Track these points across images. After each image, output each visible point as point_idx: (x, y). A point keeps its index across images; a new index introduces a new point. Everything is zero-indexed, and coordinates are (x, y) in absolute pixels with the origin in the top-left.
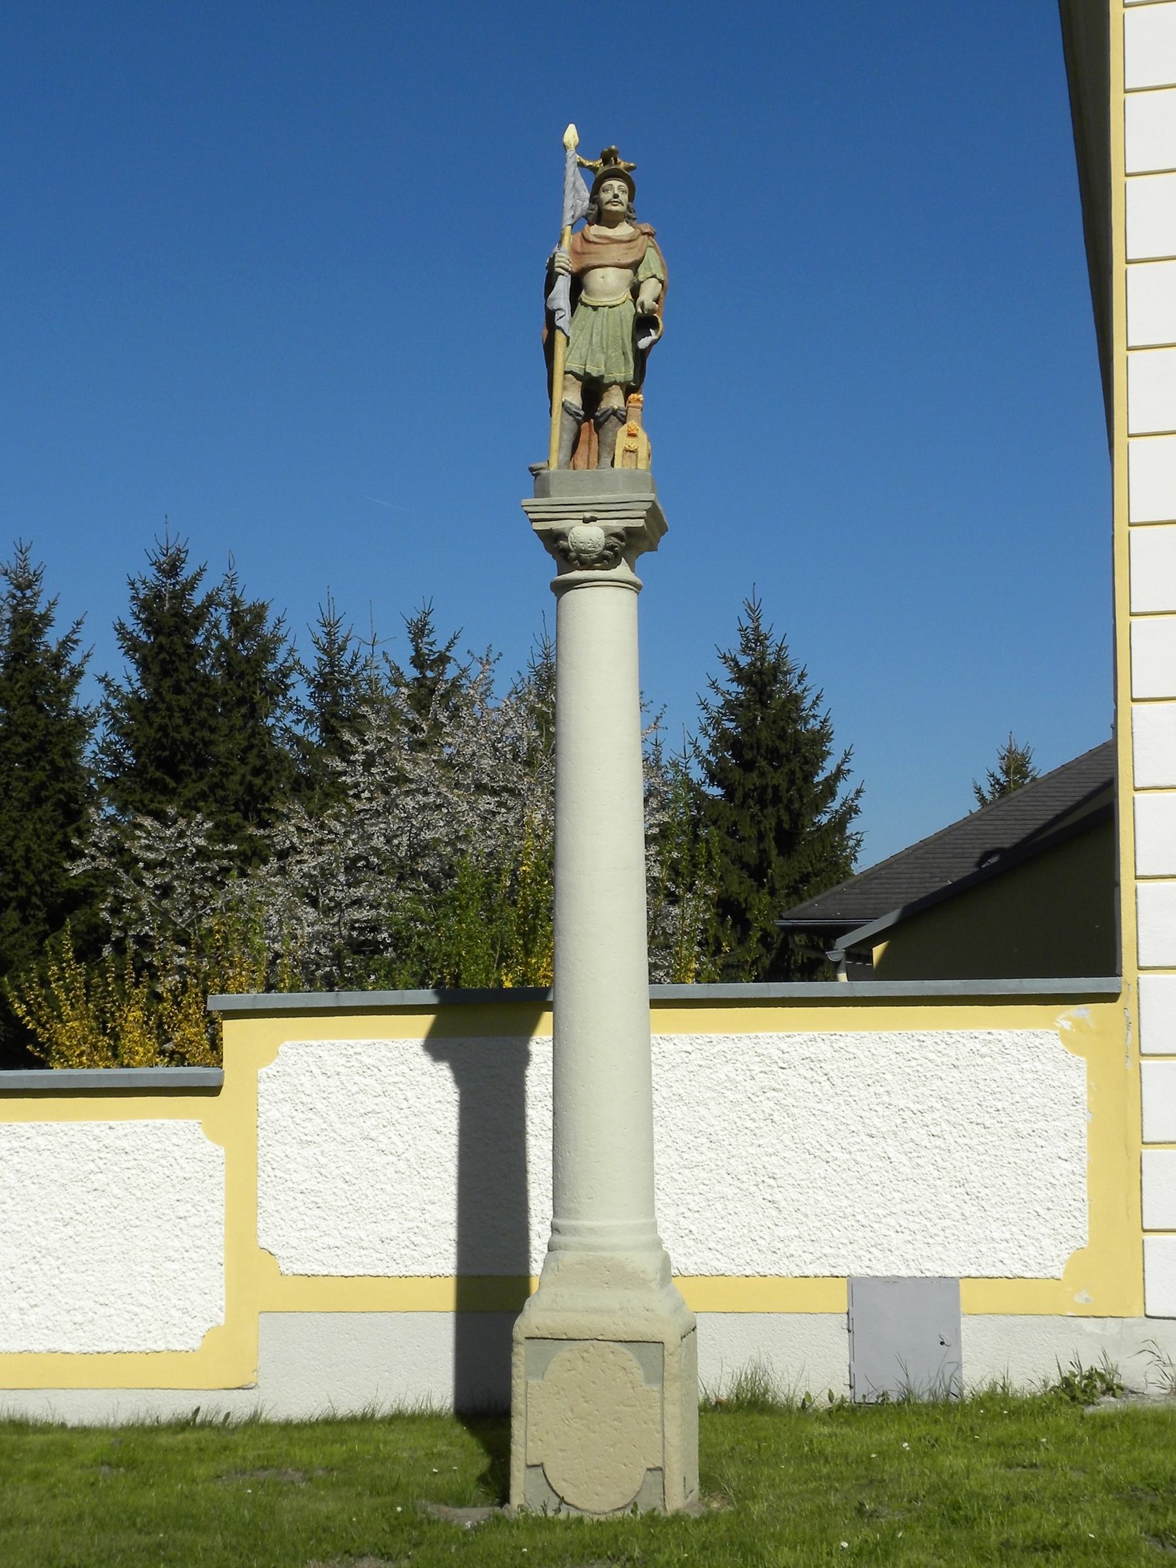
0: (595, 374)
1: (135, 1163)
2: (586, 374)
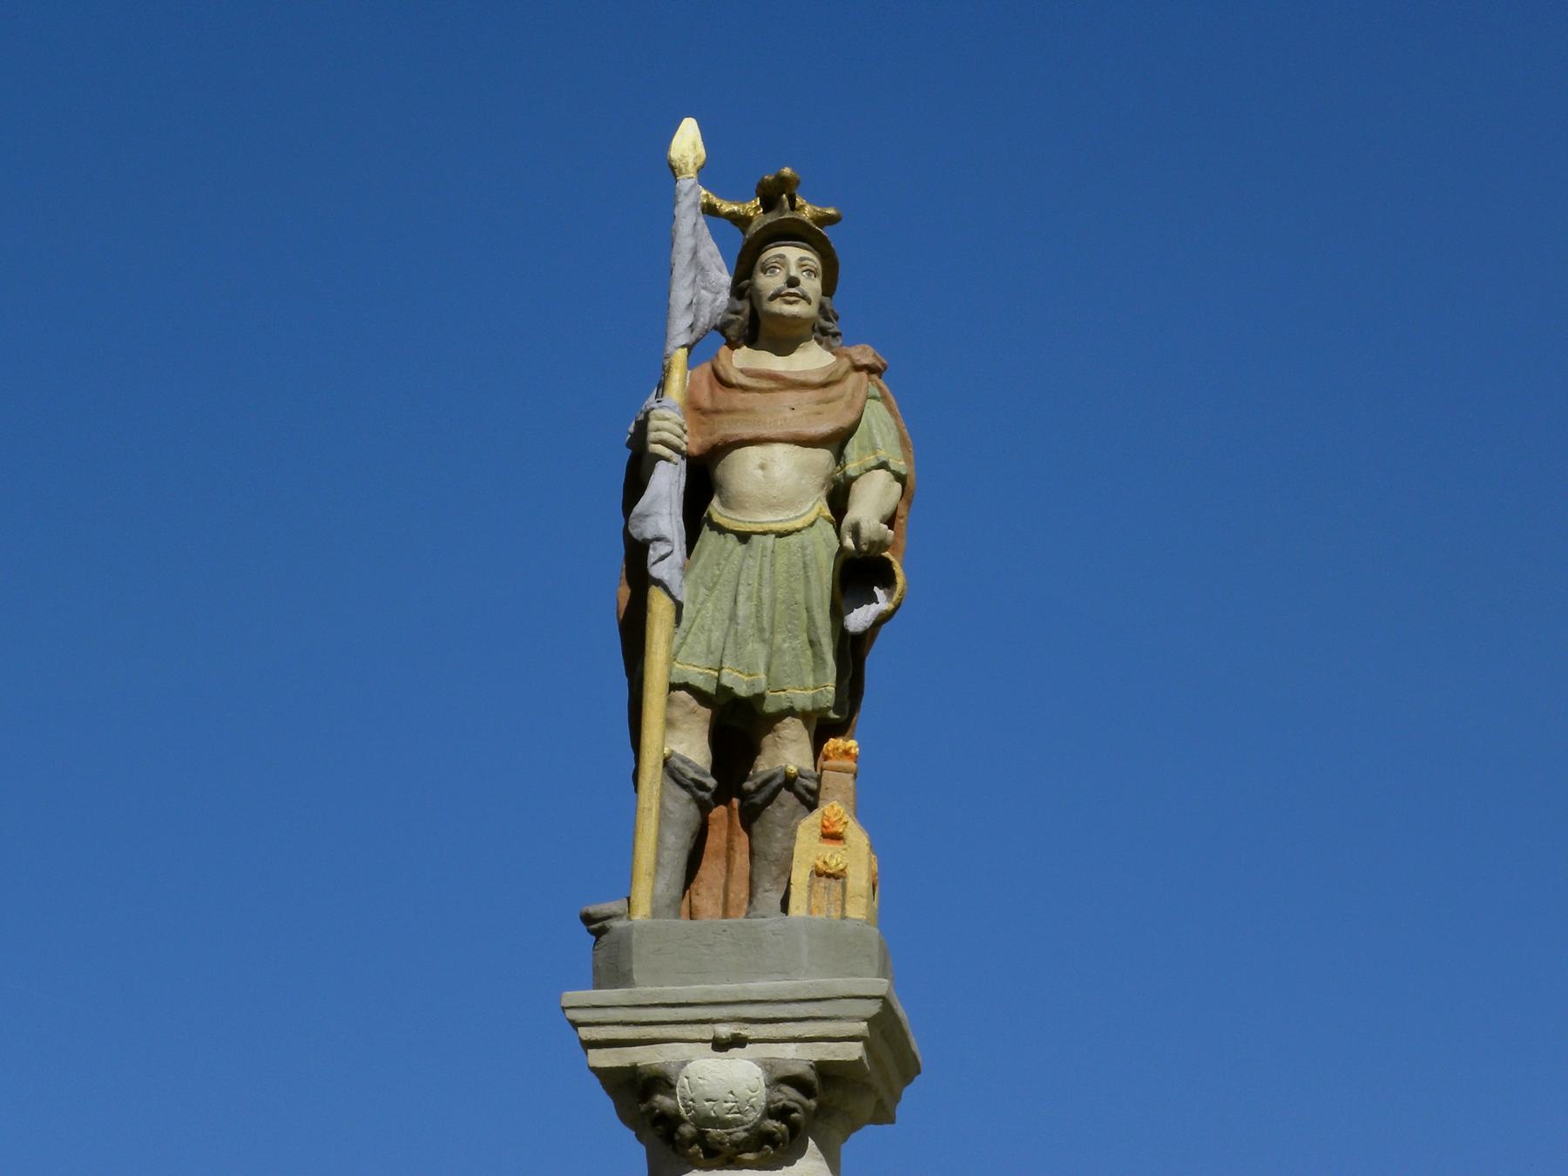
0: (742, 691)
2: (723, 690)
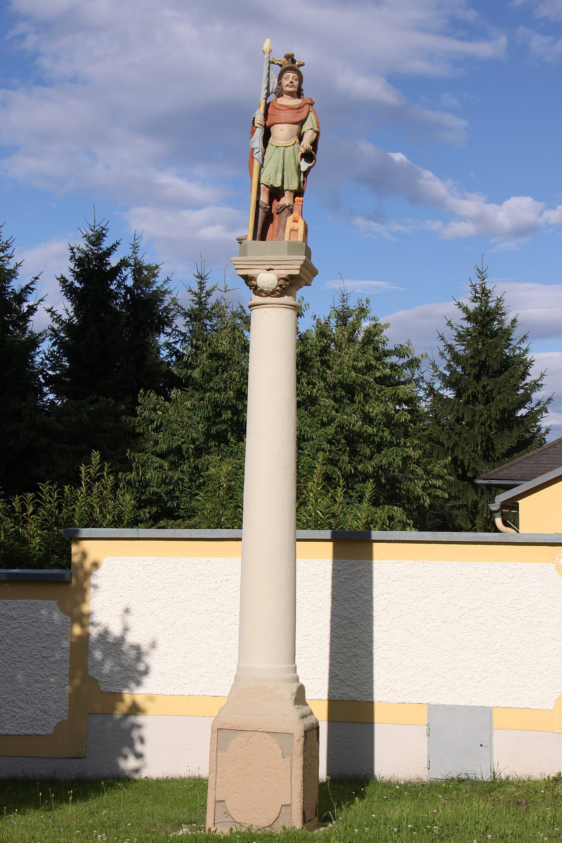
1: (18, 624)
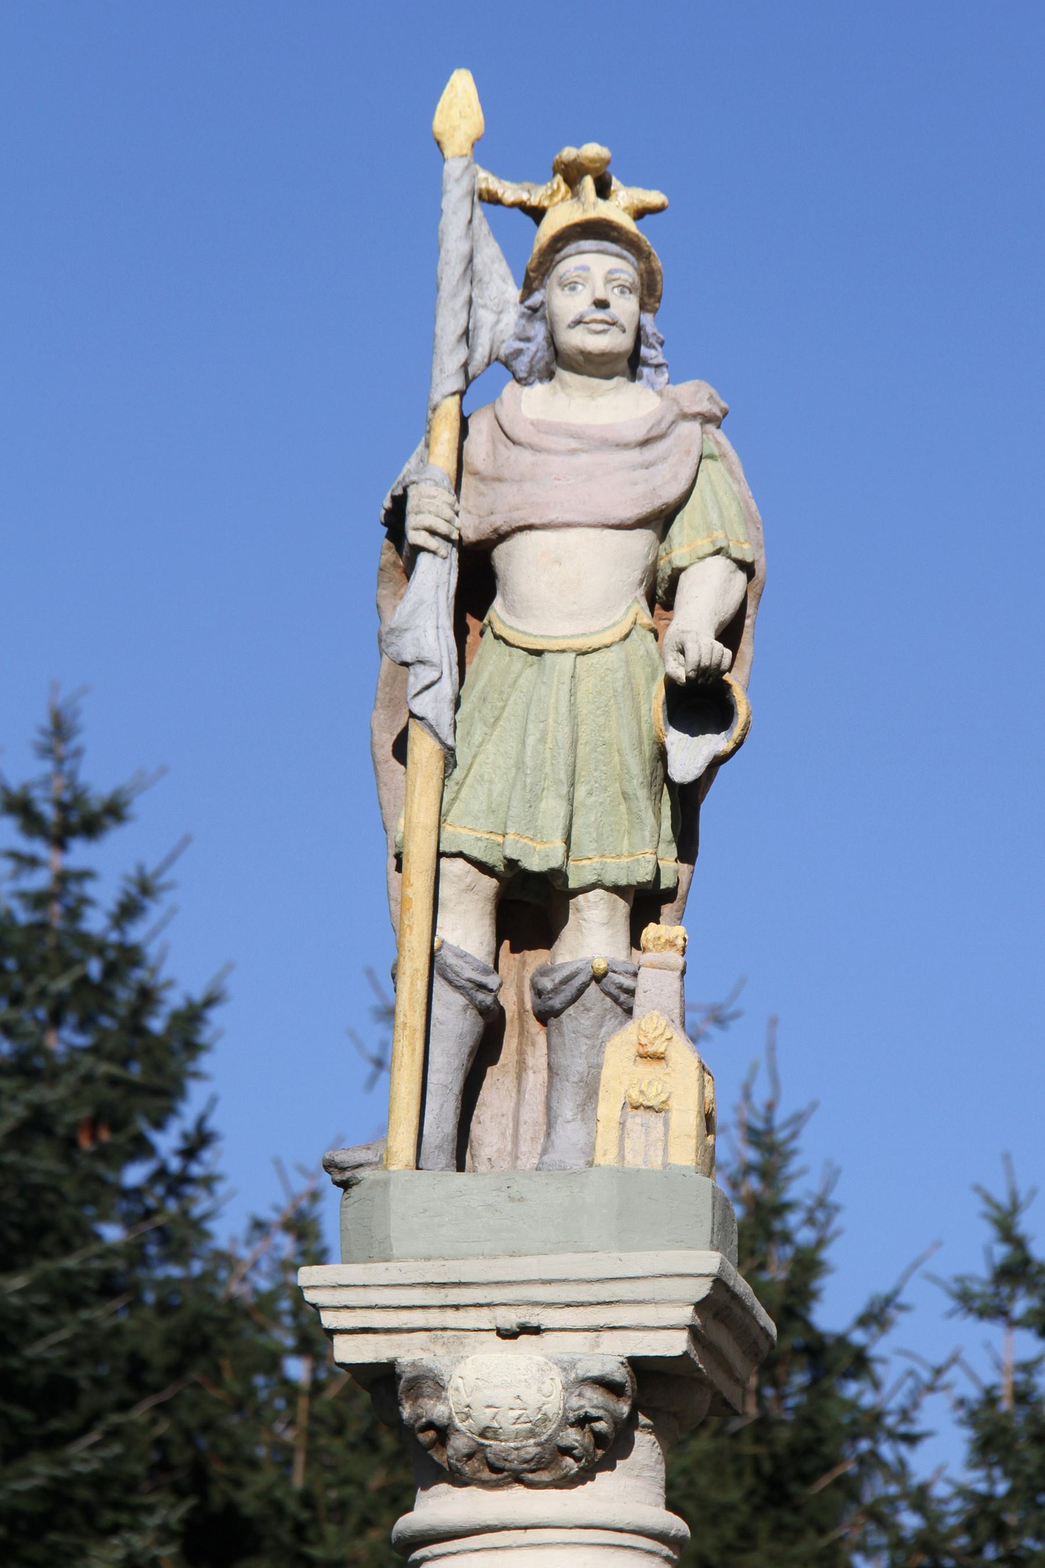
0: (534, 864)
2: (512, 863)
